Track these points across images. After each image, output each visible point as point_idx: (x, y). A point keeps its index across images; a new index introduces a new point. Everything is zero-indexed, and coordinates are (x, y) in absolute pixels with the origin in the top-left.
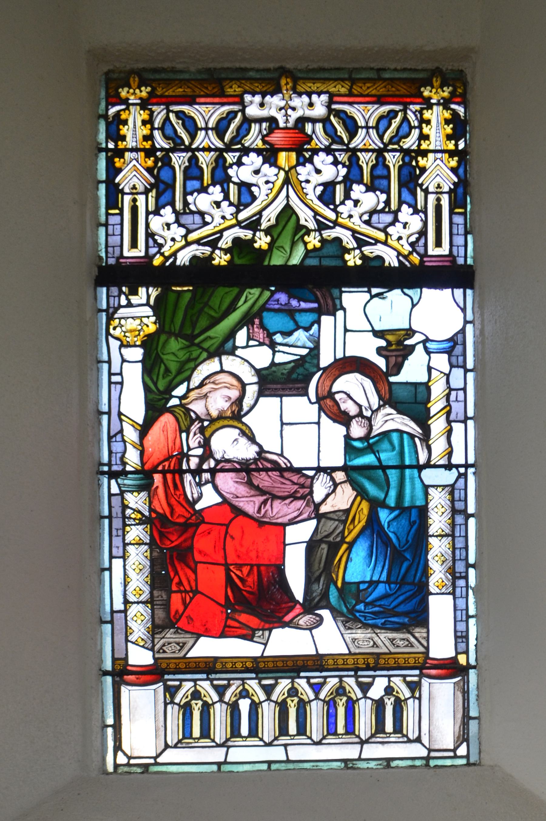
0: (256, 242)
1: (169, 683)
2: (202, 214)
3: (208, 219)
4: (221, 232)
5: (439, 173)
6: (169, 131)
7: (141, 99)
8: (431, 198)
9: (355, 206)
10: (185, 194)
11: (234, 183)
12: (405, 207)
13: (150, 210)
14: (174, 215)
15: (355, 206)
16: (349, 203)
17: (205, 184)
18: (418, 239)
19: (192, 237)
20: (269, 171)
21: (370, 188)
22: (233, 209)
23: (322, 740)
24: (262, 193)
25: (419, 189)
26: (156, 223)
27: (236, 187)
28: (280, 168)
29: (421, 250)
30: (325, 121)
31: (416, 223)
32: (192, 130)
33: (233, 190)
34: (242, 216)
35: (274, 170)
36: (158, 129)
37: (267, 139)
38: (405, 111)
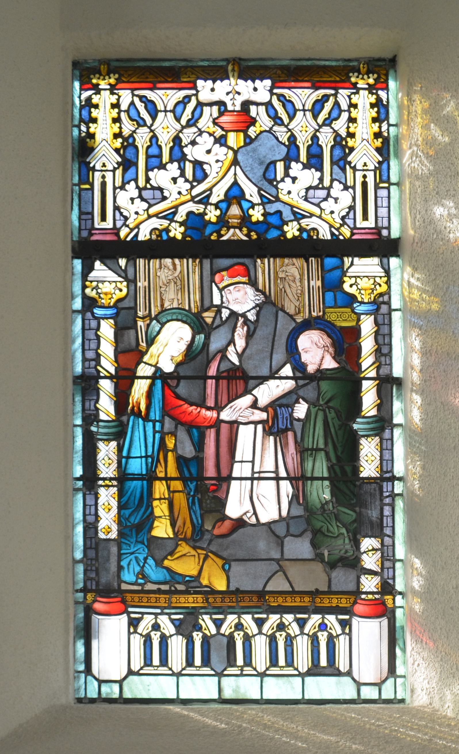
0: (206, 214)
1: (133, 616)
2: (161, 190)
3: (166, 193)
4: (176, 207)
8: (359, 175)
9: (294, 182)
10: (148, 169)
11: (190, 161)
12: (336, 183)
14: (137, 190)
15: (294, 182)
16: (288, 180)
17: (164, 162)
18: (348, 213)
19: (152, 211)
20: (220, 151)
21: (306, 166)
22: (188, 186)
23: (265, 671)
24: (213, 171)
26: (123, 199)
27: (191, 165)
28: (229, 148)
29: (350, 222)
30: (268, 105)
31: (346, 199)
32: (152, 112)
33: (189, 168)
34: (195, 192)
35: (224, 149)
36: (124, 111)
37: (216, 121)
38: (335, 95)
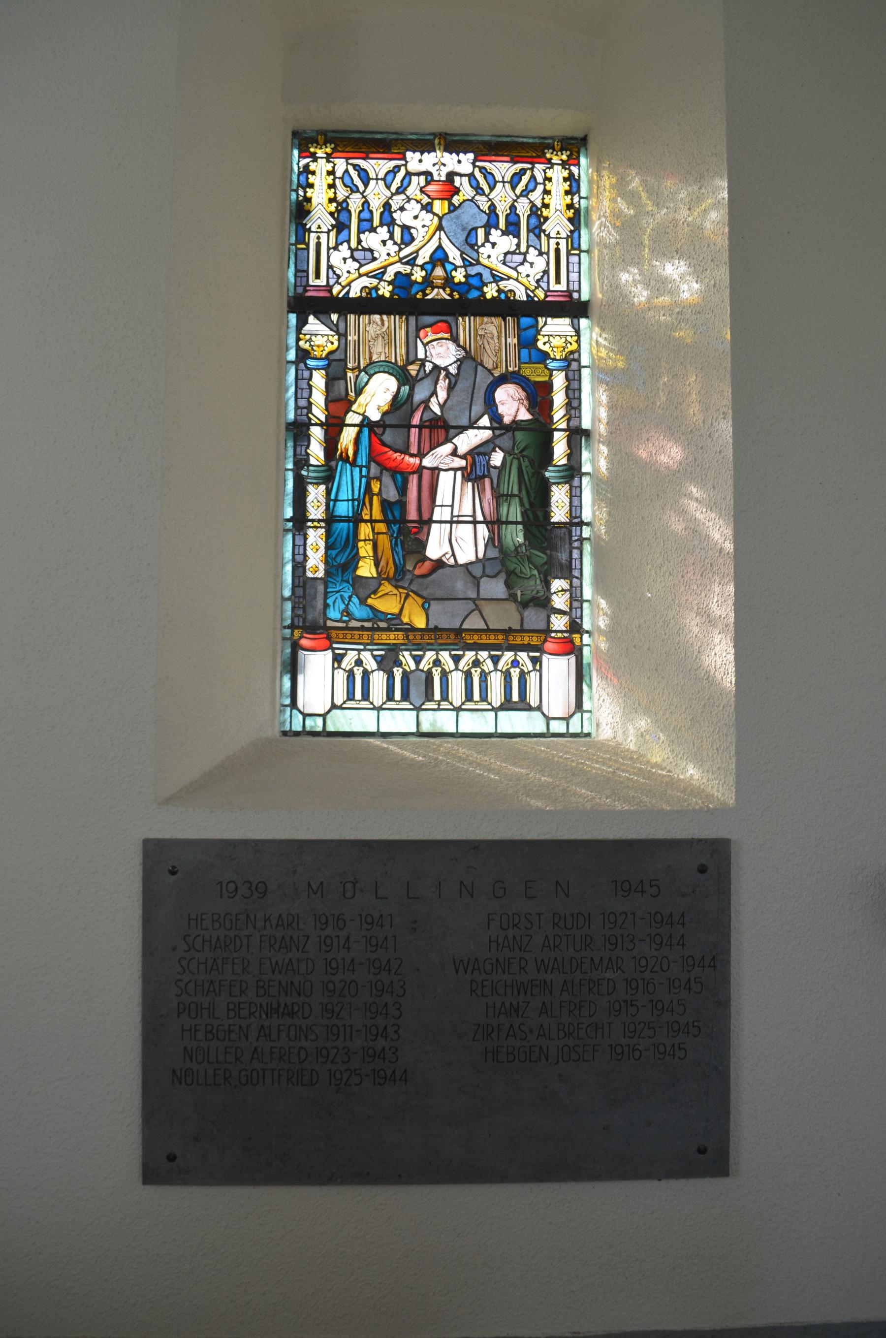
2: (371, 251)
3: (376, 255)
5: (557, 224)
6: (347, 180)
7: (326, 153)
8: (553, 242)
9: (493, 247)
10: (360, 232)
11: (399, 226)
12: (531, 249)
13: (331, 246)
15: (493, 247)
18: (542, 277)
19: (363, 270)
21: (504, 233)
22: (396, 248)
24: (420, 235)
25: (542, 234)
26: (336, 258)
27: (400, 229)
28: (435, 214)
30: (471, 176)
31: (540, 263)
33: (397, 232)
34: (402, 254)
35: (430, 216)
38: (532, 169)
